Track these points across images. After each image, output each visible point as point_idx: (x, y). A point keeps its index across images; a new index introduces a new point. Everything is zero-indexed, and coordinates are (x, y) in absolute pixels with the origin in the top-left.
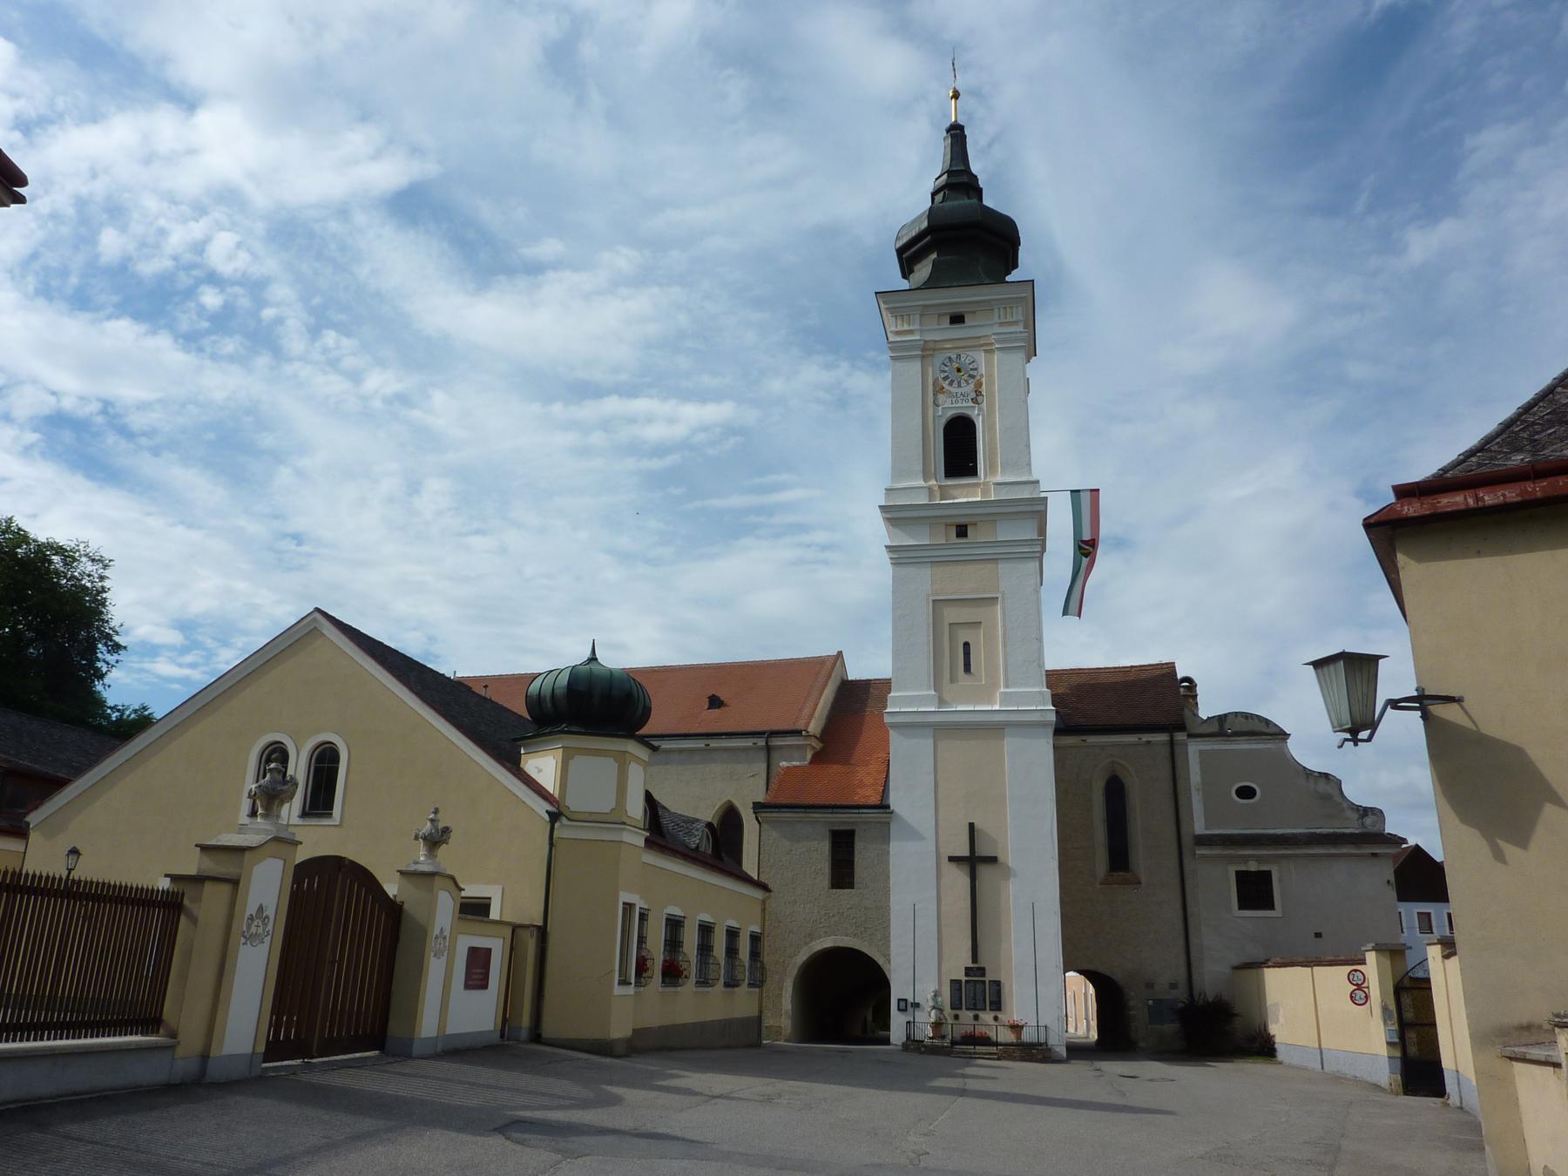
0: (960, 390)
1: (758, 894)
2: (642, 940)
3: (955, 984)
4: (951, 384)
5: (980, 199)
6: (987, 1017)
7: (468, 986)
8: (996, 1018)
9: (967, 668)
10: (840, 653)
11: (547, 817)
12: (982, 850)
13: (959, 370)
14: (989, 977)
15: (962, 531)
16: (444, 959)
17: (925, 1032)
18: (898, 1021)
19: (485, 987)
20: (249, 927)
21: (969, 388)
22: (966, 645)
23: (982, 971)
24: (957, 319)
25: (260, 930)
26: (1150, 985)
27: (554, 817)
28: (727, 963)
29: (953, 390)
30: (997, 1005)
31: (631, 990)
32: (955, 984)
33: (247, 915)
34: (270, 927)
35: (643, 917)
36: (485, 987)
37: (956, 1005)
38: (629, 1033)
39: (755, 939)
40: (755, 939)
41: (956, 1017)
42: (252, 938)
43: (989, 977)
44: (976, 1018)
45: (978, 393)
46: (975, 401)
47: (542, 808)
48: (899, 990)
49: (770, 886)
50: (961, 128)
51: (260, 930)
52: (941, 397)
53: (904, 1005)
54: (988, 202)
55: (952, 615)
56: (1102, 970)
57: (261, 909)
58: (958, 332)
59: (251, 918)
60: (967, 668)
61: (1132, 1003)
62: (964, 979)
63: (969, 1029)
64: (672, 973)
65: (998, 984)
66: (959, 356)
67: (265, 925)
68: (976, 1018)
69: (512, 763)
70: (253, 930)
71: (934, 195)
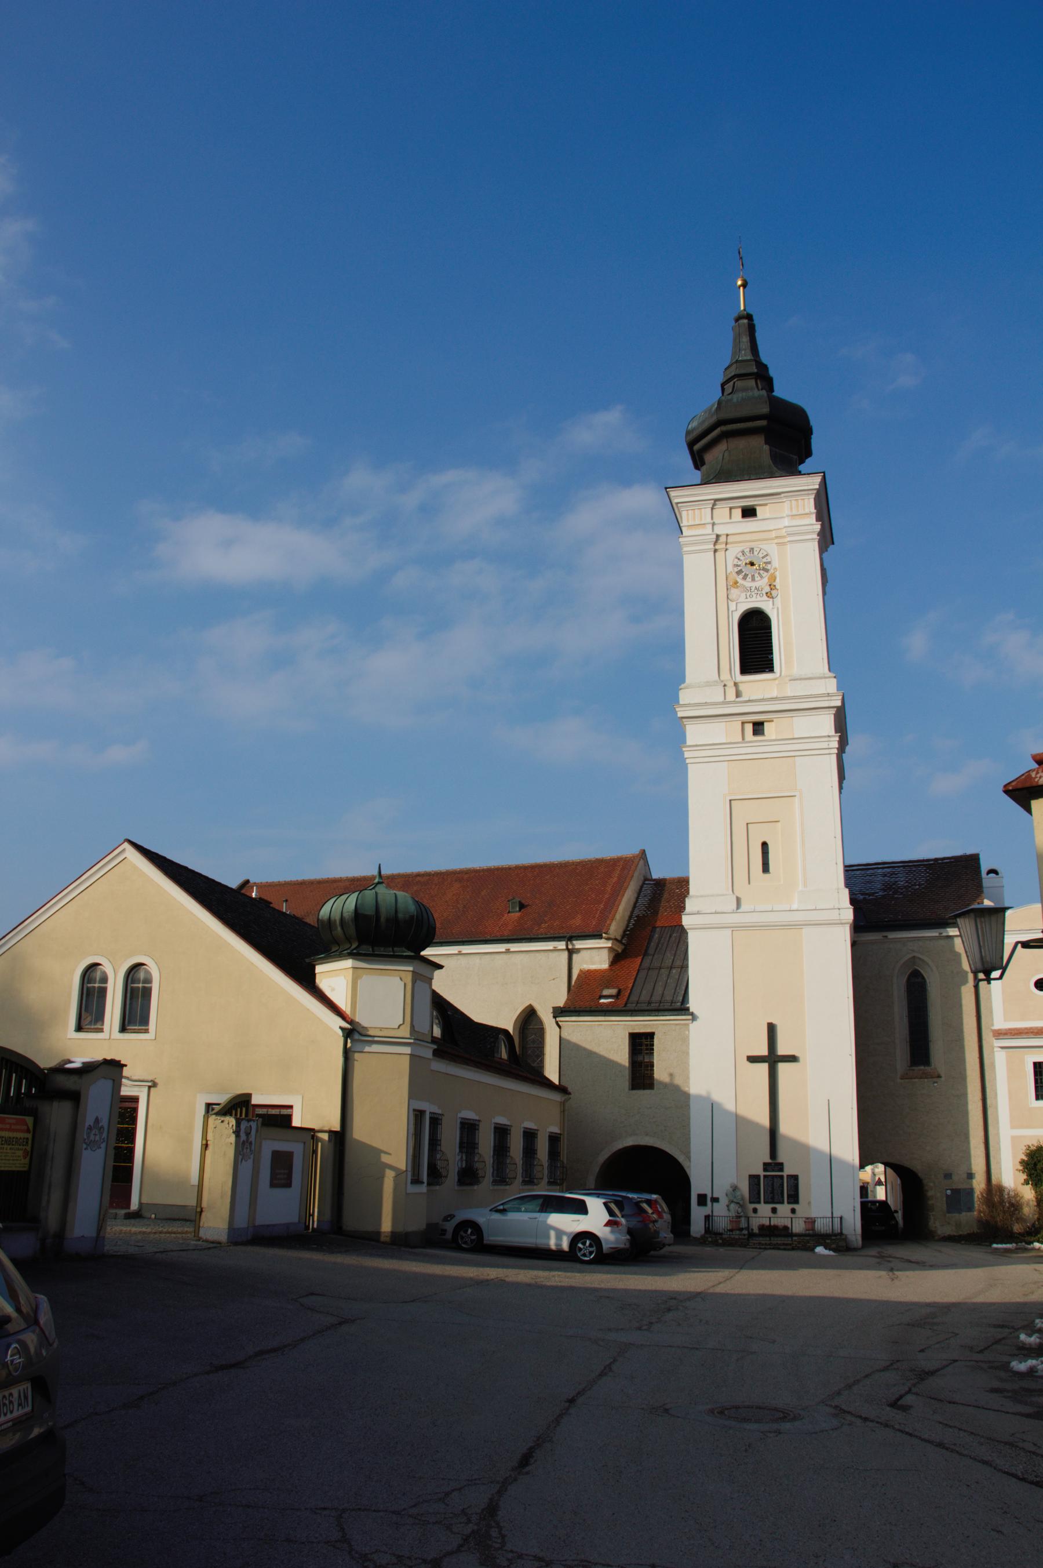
0: (753, 585)
1: (557, 1097)
2: (434, 1142)
3: (754, 1179)
4: (745, 578)
5: (771, 389)
6: (784, 1209)
7: (273, 1185)
8: (793, 1211)
9: (766, 868)
10: (643, 852)
11: (340, 1033)
12: (782, 1050)
13: (752, 564)
14: (788, 1171)
15: (758, 728)
16: (250, 1161)
17: (722, 1224)
18: (697, 1214)
19: (289, 1185)
20: (88, 1134)
21: (763, 583)
22: (764, 845)
23: (780, 1167)
24: (749, 512)
25: (97, 1138)
26: (948, 1176)
27: (348, 1034)
28: (550, 1166)
29: (748, 583)
30: (794, 1198)
31: (423, 1188)
32: (754, 1179)
33: (87, 1125)
34: (105, 1135)
35: (435, 1121)
36: (289, 1185)
37: (755, 1198)
38: (424, 1227)
39: (554, 1139)
40: (554, 1139)
41: (755, 1210)
42: (92, 1145)
43: (788, 1171)
44: (774, 1211)
45: (772, 587)
46: (769, 595)
47: (336, 1023)
48: (699, 1185)
49: (570, 1090)
50: (749, 317)
51: (97, 1138)
52: (734, 592)
53: (702, 1200)
54: (779, 392)
55: (743, 813)
56: (907, 1163)
57: (97, 1120)
58: (750, 524)
59: (90, 1128)
60: (766, 868)
61: (930, 1193)
62: (762, 1173)
63: (766, 1222)
64: (468, 1176)
65: (795, 1178)
66: (752, 550)
67: (102, 1133)
68: (774, 1211)
69: (306, 980)
70: (92, 1137)
71: (723, 386)
